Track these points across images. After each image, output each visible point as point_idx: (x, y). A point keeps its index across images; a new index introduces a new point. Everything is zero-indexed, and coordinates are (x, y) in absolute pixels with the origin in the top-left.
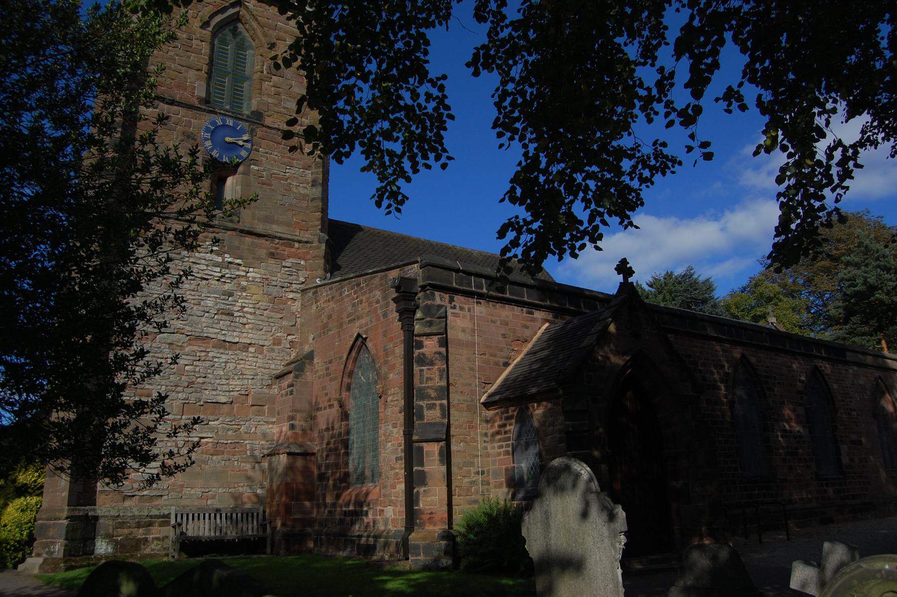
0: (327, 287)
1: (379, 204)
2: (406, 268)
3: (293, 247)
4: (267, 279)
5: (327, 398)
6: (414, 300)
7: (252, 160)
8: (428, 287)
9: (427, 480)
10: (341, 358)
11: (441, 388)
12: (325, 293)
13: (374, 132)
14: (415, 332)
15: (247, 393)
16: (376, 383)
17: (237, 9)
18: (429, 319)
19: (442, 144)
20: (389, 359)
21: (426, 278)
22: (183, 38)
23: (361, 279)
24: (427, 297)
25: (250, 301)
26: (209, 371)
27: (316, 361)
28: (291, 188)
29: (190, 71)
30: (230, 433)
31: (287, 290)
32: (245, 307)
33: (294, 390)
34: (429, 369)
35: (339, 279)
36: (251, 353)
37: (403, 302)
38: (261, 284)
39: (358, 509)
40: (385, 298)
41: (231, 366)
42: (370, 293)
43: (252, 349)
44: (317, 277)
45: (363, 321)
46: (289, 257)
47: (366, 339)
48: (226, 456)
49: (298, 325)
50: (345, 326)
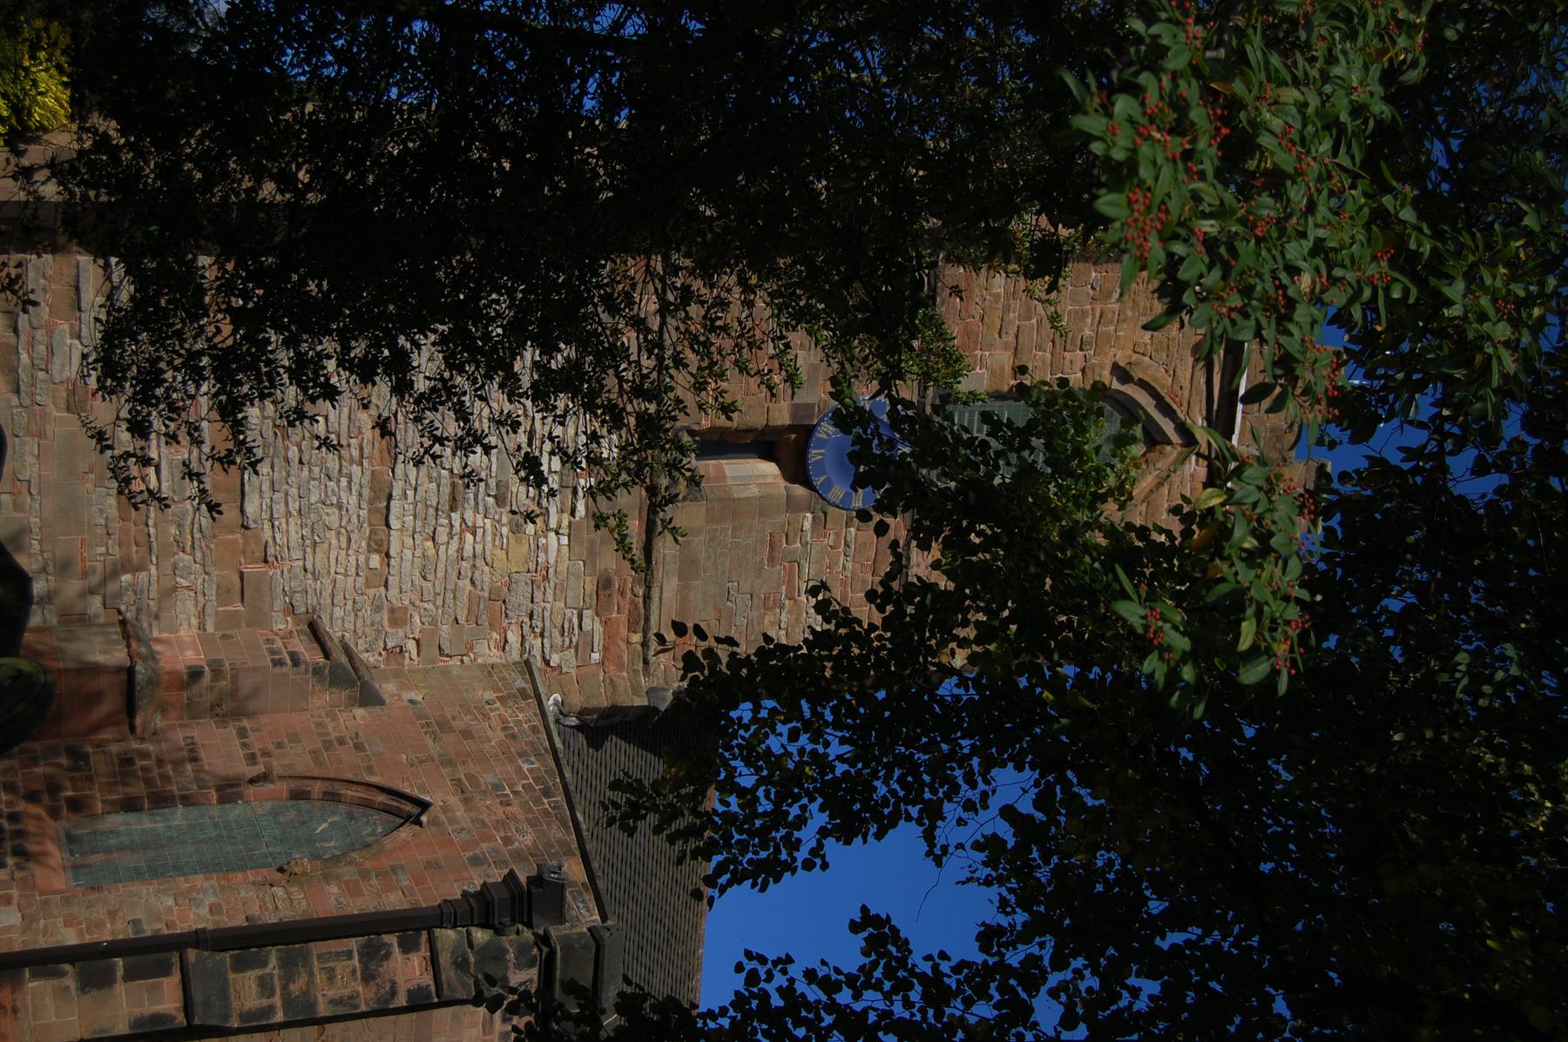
0: (537, 722)
1: (616, 785)
2: (589, 897)
3: (632, 630)
4: (546, 578)
5: (271, 747)
6: (513, 921)
7: (825, 513)
8: (545, 950)
9: (95, 993)
10: (370, 770)
11: (312, 1005)
12: (523, 716)
13: (733, 763)
14: (437, 931)
15: (270, 559)
16: (315, 857)
17: (1175, 438)
18: (472, 959)
19: (730, 883)
20: (374, 881)
21: (568, 944)
22: (1081, 330)
23: (560, 798)
24: (522, 950)
25: (489, 546)
26: (316, 470)
27: (360, 712)
28: (772, 609)
29: (1010, 353)
30: (173, 530)
31: (526, 628)
32: (474, 534)
33: (284, 669)
34: (354, 971)
35: (559, 745)
36: (367, 560)
37: (505, 895)
38: (532, 566)
39: (604, 505)
40: (518, 856)
41: (333, 517)
42: (528, 821)
43: (375, 561)
44: (563, 694)
45: (460, 812)
46: (605, 623)
47: (418, 822)
48: (116, 525)
49: (442, 662)
50: (445, 771)
